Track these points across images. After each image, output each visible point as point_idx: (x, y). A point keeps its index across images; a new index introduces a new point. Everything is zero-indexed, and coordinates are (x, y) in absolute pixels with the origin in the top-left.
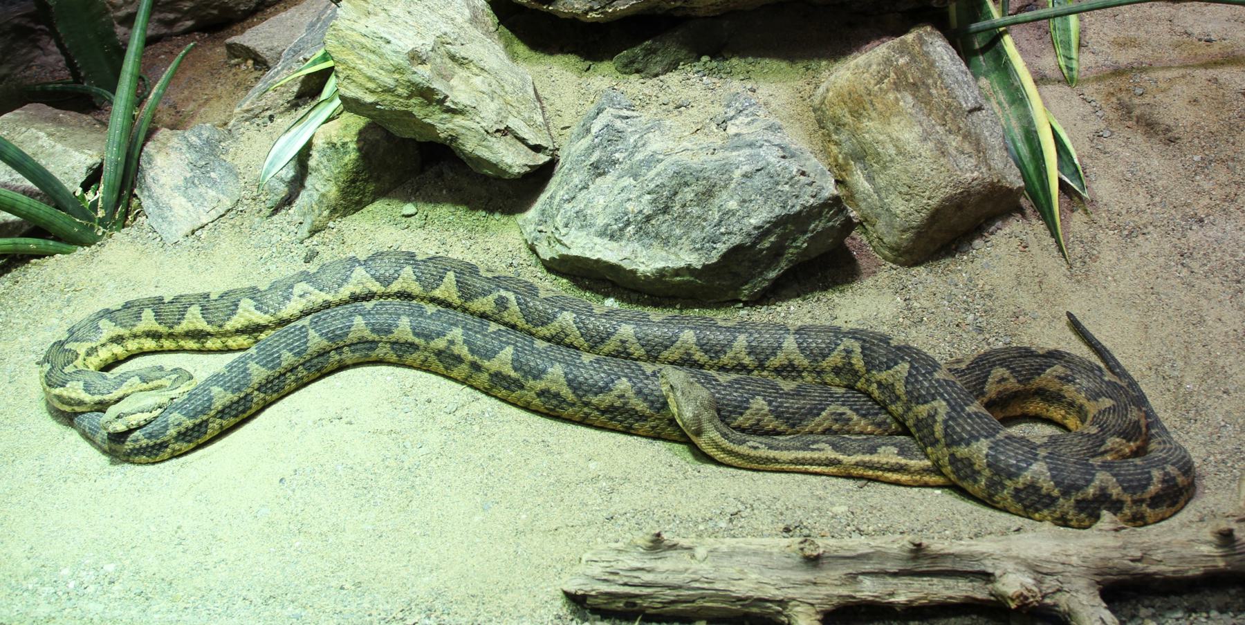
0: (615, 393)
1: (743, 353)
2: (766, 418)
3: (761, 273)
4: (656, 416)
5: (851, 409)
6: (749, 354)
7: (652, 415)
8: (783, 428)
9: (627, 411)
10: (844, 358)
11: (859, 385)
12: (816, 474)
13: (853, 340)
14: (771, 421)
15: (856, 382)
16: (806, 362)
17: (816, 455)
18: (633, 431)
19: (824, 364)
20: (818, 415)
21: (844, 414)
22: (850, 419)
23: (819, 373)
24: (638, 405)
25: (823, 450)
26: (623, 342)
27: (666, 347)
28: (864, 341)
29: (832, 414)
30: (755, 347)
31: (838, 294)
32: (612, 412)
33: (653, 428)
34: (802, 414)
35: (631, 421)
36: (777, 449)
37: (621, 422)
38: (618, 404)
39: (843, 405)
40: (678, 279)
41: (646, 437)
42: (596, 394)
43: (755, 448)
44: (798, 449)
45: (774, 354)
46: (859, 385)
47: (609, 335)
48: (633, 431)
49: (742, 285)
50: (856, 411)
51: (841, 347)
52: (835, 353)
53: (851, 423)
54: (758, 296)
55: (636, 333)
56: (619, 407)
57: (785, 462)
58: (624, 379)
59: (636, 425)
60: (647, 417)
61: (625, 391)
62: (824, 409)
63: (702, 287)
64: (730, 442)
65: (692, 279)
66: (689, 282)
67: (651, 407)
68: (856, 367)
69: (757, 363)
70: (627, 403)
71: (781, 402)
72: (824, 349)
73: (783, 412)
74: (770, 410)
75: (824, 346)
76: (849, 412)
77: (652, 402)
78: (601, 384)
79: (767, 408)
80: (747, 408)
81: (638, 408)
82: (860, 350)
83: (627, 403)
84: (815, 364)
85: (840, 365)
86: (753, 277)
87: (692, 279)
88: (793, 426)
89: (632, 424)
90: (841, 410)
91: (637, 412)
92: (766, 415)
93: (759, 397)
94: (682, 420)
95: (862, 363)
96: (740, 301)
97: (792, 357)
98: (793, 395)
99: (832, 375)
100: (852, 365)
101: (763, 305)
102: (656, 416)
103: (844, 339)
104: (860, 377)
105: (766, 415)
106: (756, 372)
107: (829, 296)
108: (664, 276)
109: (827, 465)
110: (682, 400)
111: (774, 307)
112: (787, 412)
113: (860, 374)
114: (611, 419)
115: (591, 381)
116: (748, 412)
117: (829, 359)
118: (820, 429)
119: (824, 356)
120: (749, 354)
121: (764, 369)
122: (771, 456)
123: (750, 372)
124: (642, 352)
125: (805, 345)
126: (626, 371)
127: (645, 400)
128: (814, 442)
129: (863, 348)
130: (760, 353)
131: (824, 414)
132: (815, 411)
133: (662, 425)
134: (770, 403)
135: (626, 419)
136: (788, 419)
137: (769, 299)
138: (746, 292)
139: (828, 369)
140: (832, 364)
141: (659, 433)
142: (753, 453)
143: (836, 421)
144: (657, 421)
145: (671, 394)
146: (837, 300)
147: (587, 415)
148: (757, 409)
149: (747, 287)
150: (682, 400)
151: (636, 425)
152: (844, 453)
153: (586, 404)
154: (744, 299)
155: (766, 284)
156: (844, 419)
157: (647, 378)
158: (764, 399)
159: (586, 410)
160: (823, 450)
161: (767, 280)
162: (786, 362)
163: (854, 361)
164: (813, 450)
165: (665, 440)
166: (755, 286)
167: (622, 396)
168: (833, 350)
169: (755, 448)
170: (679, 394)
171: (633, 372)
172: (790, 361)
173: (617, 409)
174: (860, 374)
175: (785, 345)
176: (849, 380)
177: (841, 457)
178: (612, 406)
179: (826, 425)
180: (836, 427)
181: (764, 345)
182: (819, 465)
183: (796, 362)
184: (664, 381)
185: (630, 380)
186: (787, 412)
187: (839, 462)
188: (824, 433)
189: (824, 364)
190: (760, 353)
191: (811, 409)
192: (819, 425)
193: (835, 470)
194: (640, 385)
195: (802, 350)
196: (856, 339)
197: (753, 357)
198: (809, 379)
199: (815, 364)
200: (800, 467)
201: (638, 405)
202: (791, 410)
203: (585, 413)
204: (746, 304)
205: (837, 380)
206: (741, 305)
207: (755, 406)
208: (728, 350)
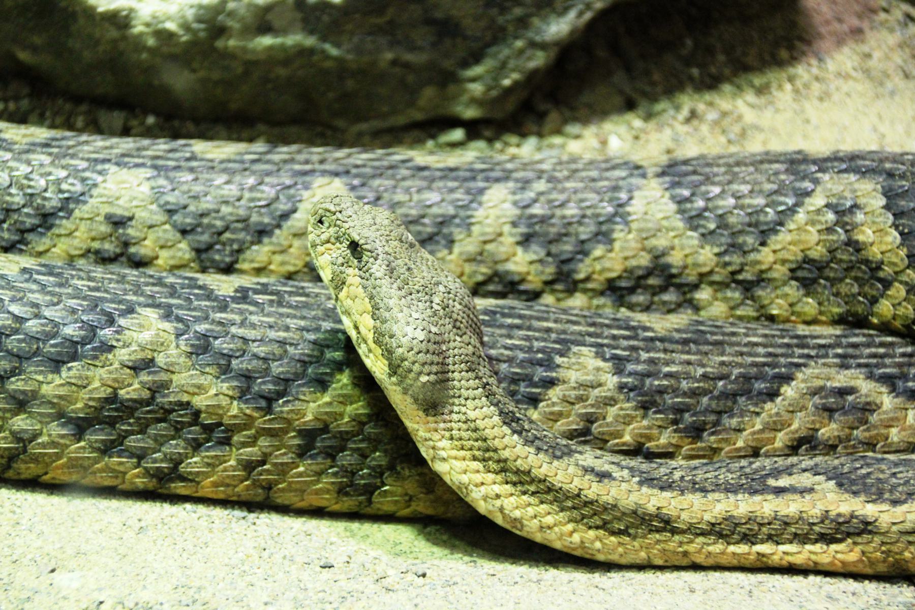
0: (123, 355)
1: (508, 240)
2: (612, 411)
3: (523, 23)
4: (261, 422)
5: (870, 377)
6: (526, 241)
7: (248, 422)
8: (665, 439)
9: (165, 414)
10: (829, 230)
11: (885, 308)
12: (791, 570)
13: (852, 177)
14: (627, 420)
15: (874, 301)
16: (707, 256)
17: (790, 507)
18: (179, 488)
19: (766, 256)
20: (772, 395)
21: (851, 391)
22: (869, 408)
23: (748, 287)
24: (201, 389)
25: (811, 490)
26: (118, 222)
27: (262, 233)
28: (890, 175)
29: (815, 392)
30: (543, 220)
31: (750, 97)
32: (112, 423)
33: (249, 466)
34: (724, 395)
35: (175, 447)
36: (666, 486)
37: (140, 456)
38: (133, 390)
39: (844, 366)
40: (267, 41)
41: (225, 503)
42: (56, 364)
43: (603, 476)
44: (730, 489)
45: (603, 236)
46: (885, 308)
47: (68, 205)
48: (179, 488)
49: (466, 64)
50: (889, 381)
51: (818, 201)
52: (801, 216)
53: (874, 418)
54: (511, 105)
55: (158, 194)
56: (141, 402)
57: (694, 531)
58: (151, 314)
59: (194, 463)
60: (232, 430)
61: (159, 346)
62: (787, 379)
63: (342, 69)
64: (528, 442)
65: (310, 41)
66: (304, 53)
67: (243, 394)
68: (875, 253)
69: (550, 270)
70: (165, 385)
71: (652, 361)
72: (761, 211)
73: (661, 391)
74: (621, 387)
75: (760, 201)
76: (866, 387)
77: (247, 377)
78: (71, 331)
79: (612, 381)
80: (551, 383)
81: (199, 402)
82: (883, 201)
83: (165, 385)
84: (736, 259)
85: (818, 252)
86: (498, 36)
87: (310, 41)
88: (696, 432)
89: (177, 462)
90: (841, 379)
91: (197, 413)
92: (610, 401)
93: (584, 350)
94: (388, 353)
95: (894, 237)
96: (454, 122)
97: (661, 242)
98: (685, 342)
99: (792, 290)
100: (857, 247)
101: (524, 135)
102: (261, 422)
103: (826, 177)
104: (887, 284)
105: (610, 401)
106: (548, 299)
107: (724, 103)
108: (219, 31)
109: (827, 539)
110: (389, 291)
111: (557, 140)
112: (675, 391)
113: (888, 270)
114: (106, 449)
115: (33, 326)
116: (554, 394)
117: (782, 238)
118: (781, 440)
119: (765, 233)
120: (526, 241)
121: (573, 287)
122: (651, 508)
123: (535, 296)
124: (184, 250)
125: (700, 203)
126: (148, 290)
127: (225, 370)
128: (777, 473)
129: (888, 193)
130: (559, 238)
131: (789, 391)
132: (760, 386)
133: (282, 457)
134: (619, 365)
135: (160, 441)
136: (680, 410)
137: (541, 117)
138: (477, 88)
139: (780, 272)
140: (794, 254)
141: (269, 487)
142: (593, 490)
143: (829, 411)
144: (264, 442)
145: (352, 275)
146: (749, 116)
147: (23, 440)
148: (581, 385)
149: (477, 70)
150: (389, 291)
151: (194, 463)
152: (878, 496)
153: (21, 404)
154: (470, 113)
155: (538, 60)
156: (854, 407)
157: (224, 308)
158: (600, 355)
159: (20, 422)
160: (811, 490)
161: (543, 46)
162: (644, 260)
163: (866, 235)
164: (779, 491)
165: (284, 510)
166: (503, 67)
167: (146, 364)
168: (792, 210)
169: (603, 476)
170: (378, 269)
171: (173, 293)
172: (658, 256)
173: (129, 409)
174: (888, 270)
175: (636, 207)
176: (850, 299)
177: (870, 510)
178: (113, 399)
179: (798, 424)
180: (829, 430)
181: (571, 211)
182: (802, 539)
183: (675, 259)
184: (328, 232)
185: (168, 315)
186: (675, 391)
187: (866, 528)
188: (794, 449)
189: (766, 256)
190: (559, 238)
191: (747, 378)
192: (774, 427)
193: (853, 557)
194: (202, 328)
195: (693, 220)
196: (864, 173)
197: (536, 252)
198: (718, 309)
199: (736, 259)
200: (742, 549)
201: (201, 389)
202: (685, 385)
203: (17, 437)
204: (474, 129)
205: (810, 306)
206: (458, 134)
207: (573, 376)
208: (458, 234)
